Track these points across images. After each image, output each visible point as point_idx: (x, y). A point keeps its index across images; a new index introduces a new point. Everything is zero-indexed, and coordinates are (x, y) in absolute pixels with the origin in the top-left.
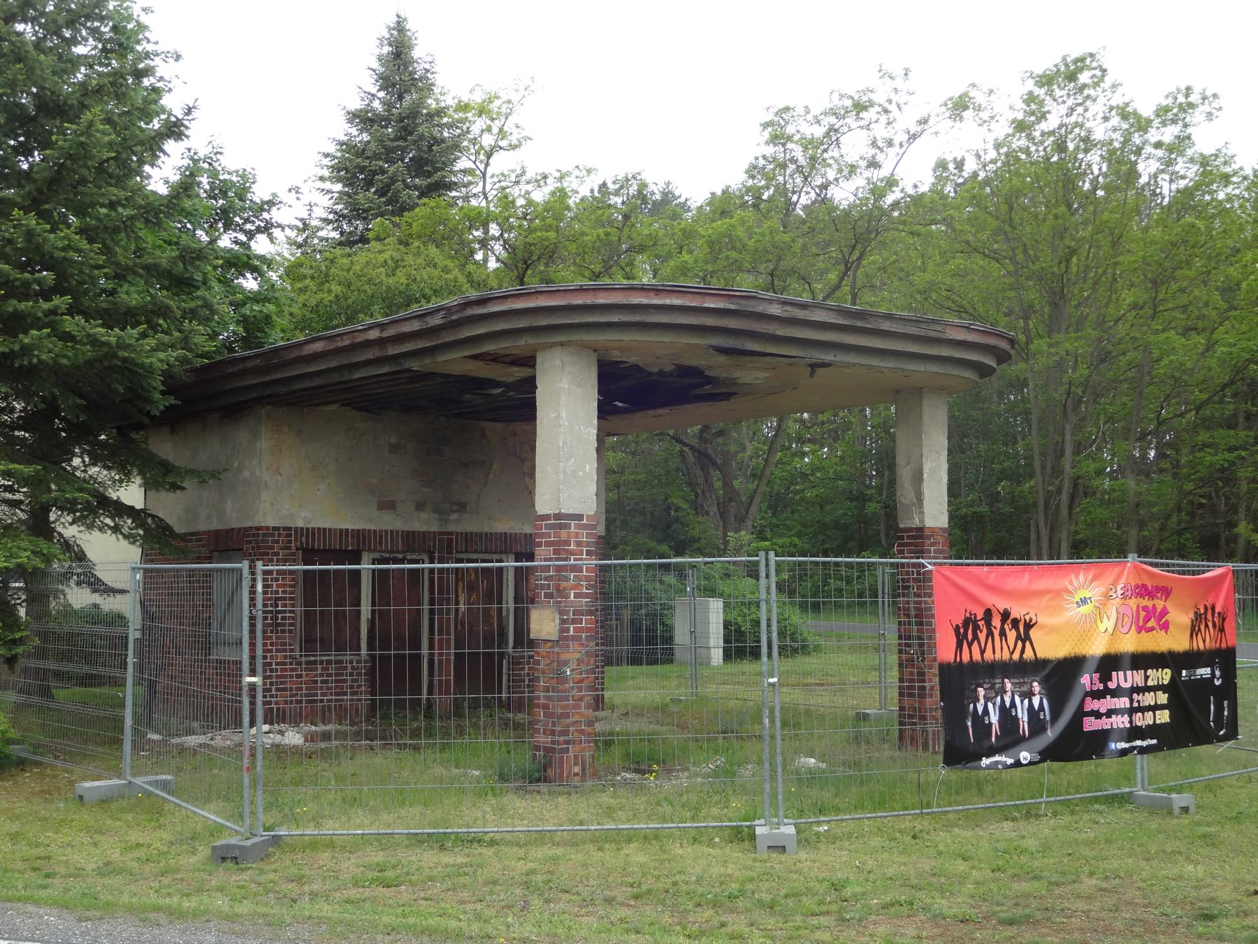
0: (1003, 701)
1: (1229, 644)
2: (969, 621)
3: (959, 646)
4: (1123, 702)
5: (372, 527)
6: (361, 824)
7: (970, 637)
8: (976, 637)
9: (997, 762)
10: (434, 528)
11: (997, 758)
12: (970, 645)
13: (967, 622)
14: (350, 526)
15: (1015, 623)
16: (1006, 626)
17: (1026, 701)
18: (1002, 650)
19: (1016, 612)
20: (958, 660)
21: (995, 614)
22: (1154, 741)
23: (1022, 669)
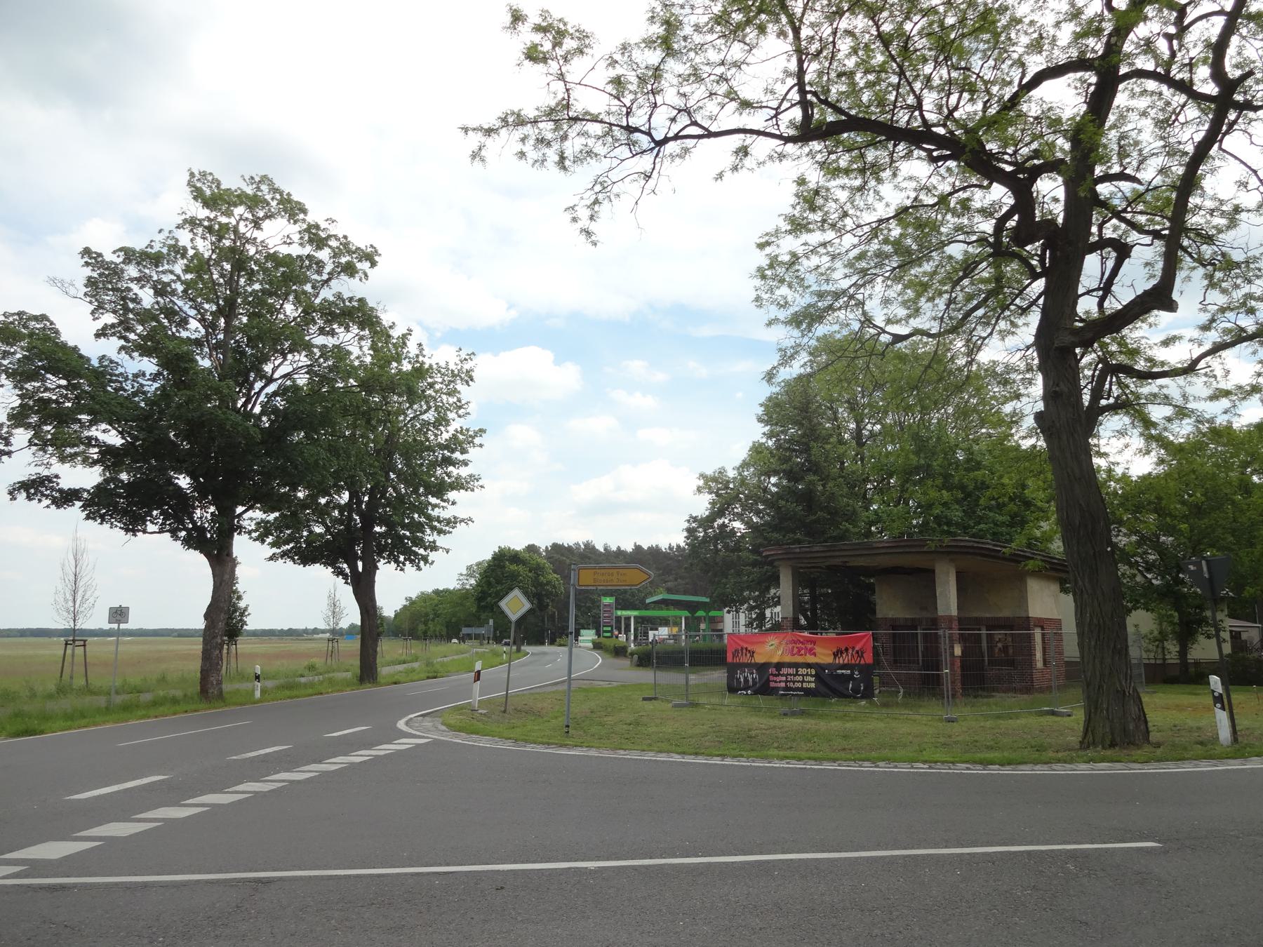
2: (737, 651)
4: (784, 678)
6: (907, 712)
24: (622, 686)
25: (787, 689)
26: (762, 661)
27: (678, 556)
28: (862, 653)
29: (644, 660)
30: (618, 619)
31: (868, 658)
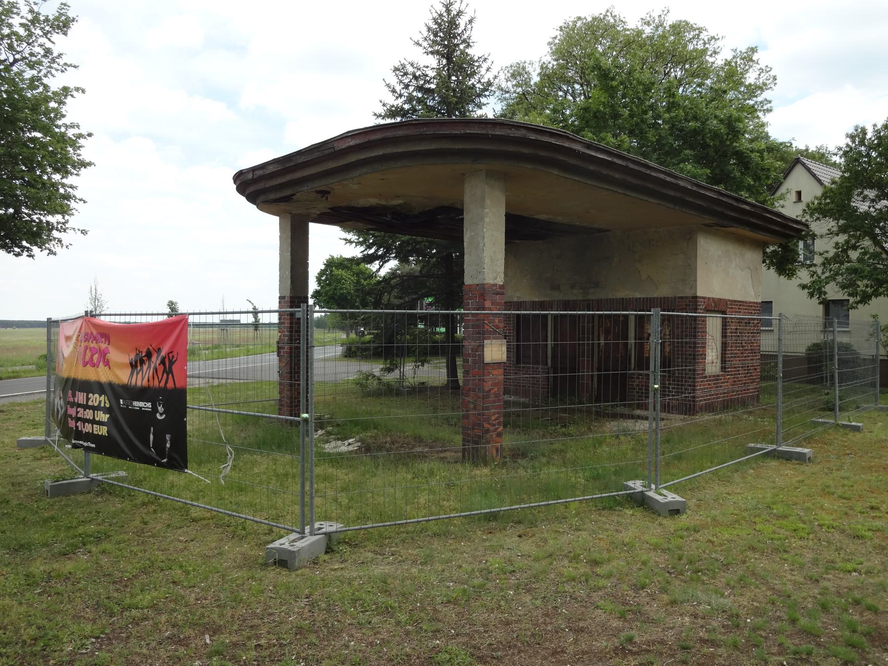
1: (178, 385)
5: (548, 299)
10: (580, 298)
14: (537, 300)
22: (94, 446)
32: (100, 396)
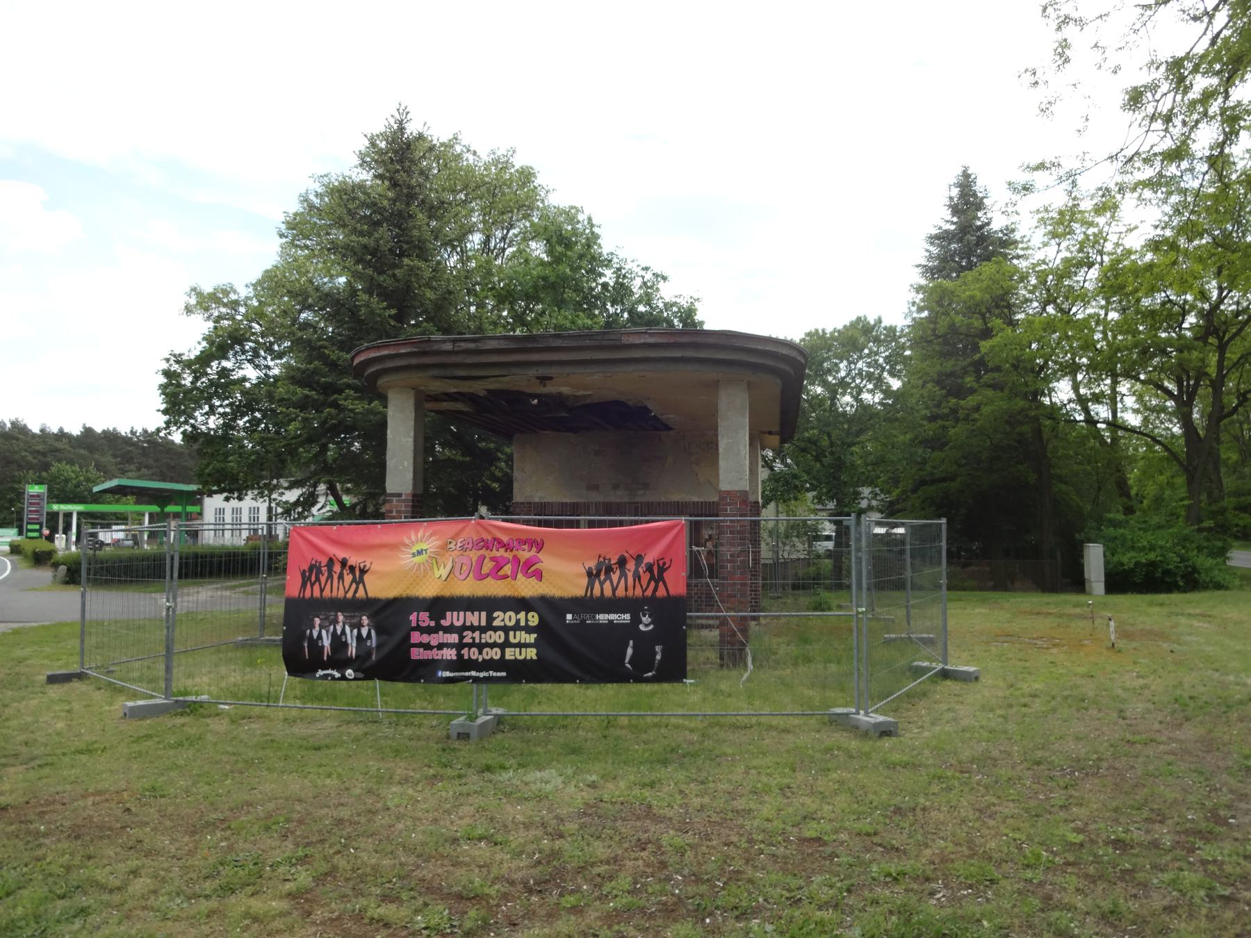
0: (335, 629)
2: (314, 568)
3: (304, 586)
4: (453, 638)
5: (583, 501)
7: (313, 579)
8: (318, 579)
9: (329, 675)
10: (626, 500)
11: (329, 671)
12: (312, 585)
13: (311, 568)
14: (568, 500)
15: (352, 569)
16: (345, 572)
17: (355, 631)
18: (340, 589)
19: (354, 560)
20: (589, 594)
21: (336, 562)
22: (504, 674)
23: (354, 607)
24: (16, 632)
25: (461, 664)
26: (391, 593)
27: (144, 442)
28: (662, 570)
29: (73, 575)
30: (53, 516)
31: (676, 582)
32: (517, 613)
